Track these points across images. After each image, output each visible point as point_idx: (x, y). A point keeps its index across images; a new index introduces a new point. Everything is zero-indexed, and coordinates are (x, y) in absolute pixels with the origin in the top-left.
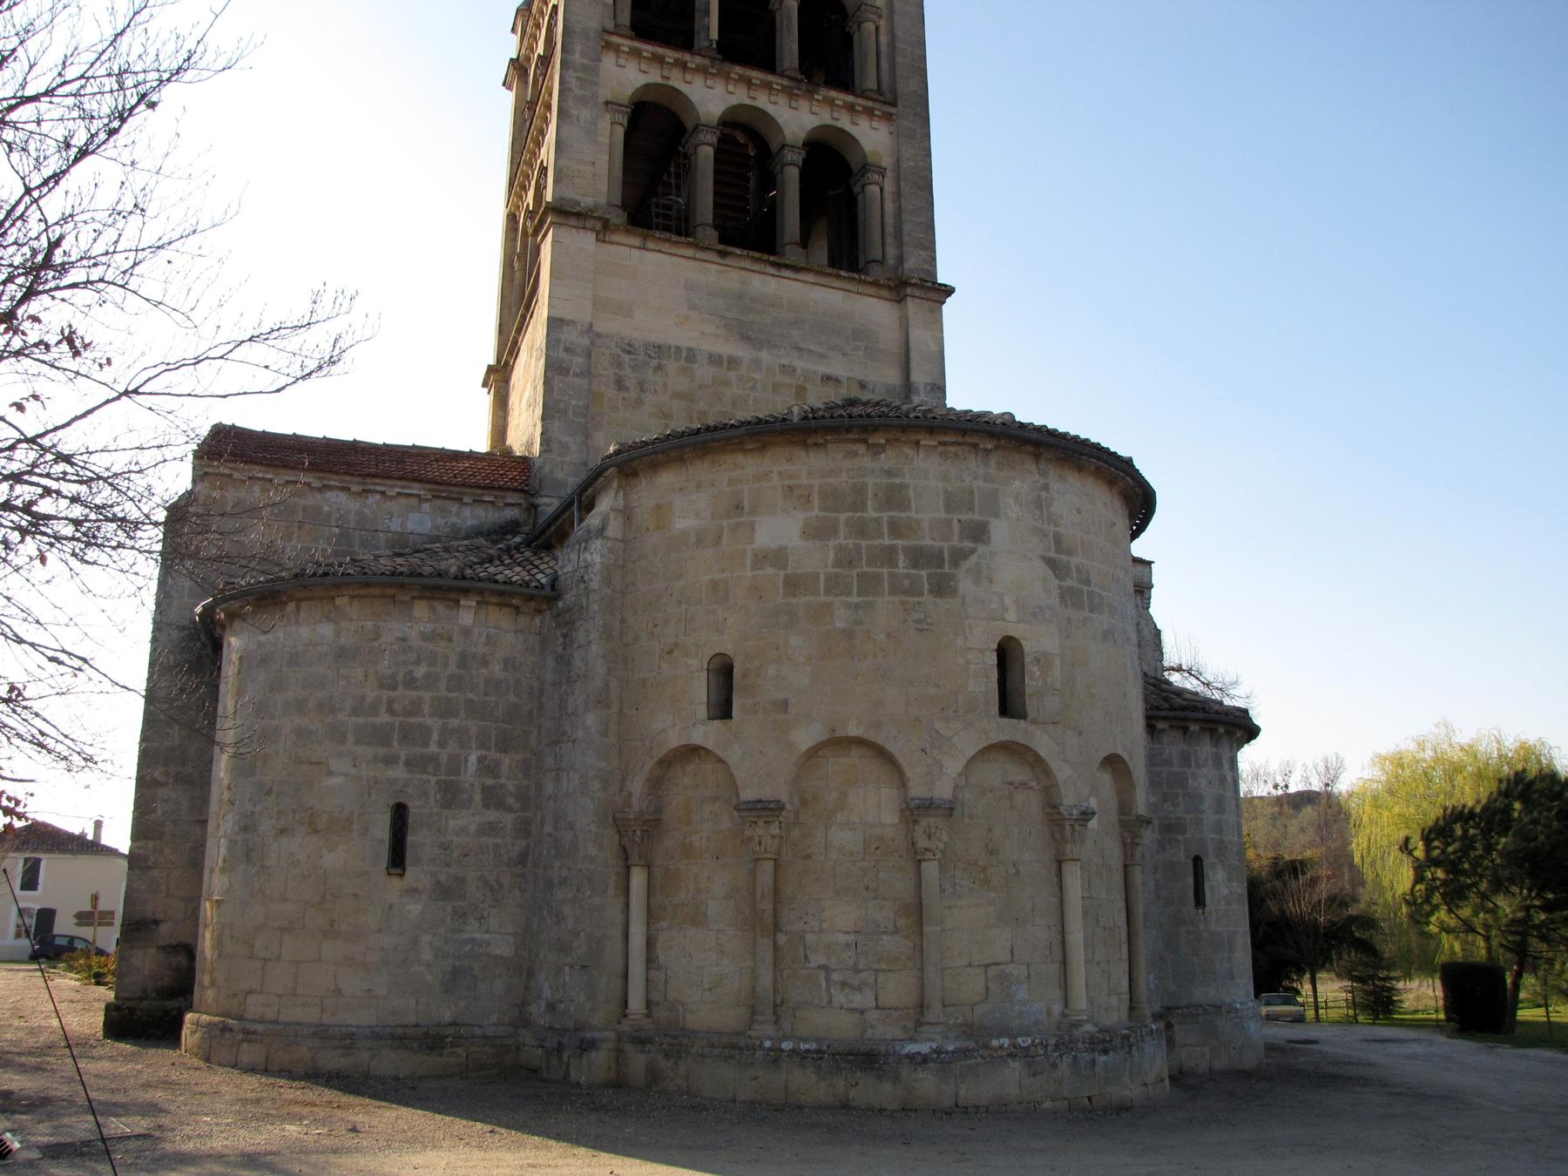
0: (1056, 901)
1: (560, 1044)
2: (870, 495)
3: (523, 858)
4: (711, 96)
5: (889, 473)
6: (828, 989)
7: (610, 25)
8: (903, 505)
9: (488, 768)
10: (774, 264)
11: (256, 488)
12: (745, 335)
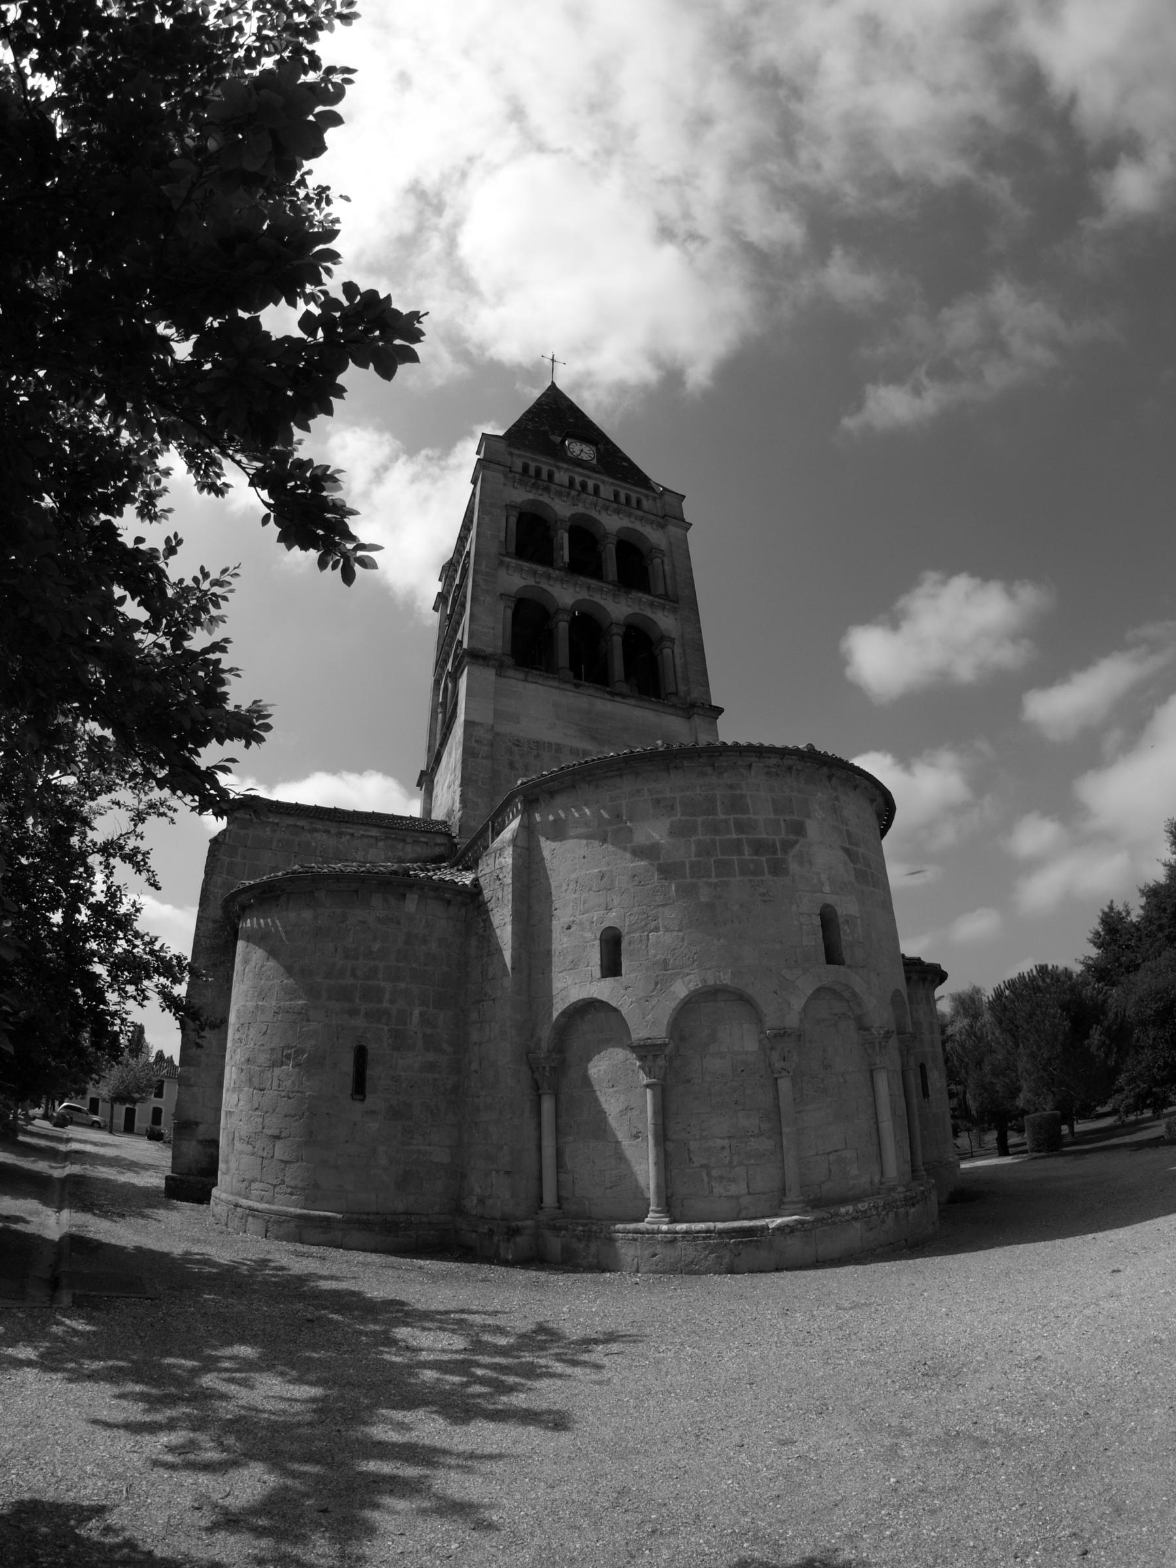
0: (870, 1099)
1: (490, 1230)
2: (718, 804)
4: (566, 594)
5: (731, 787)
6: (709, 1182)
10: (609, 693)
11: (268, 829)
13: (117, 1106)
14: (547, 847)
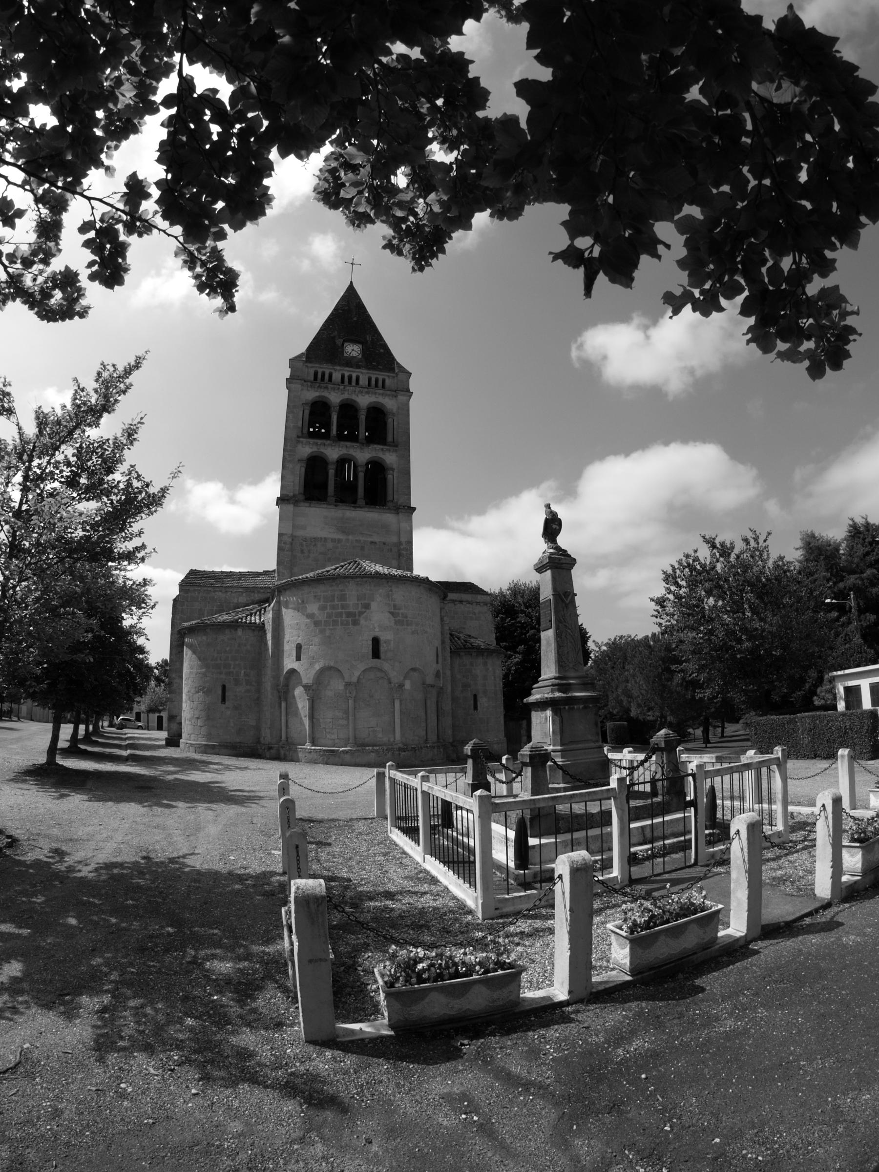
3: (258, 699)
5: (341, 591)
7: (300, 434)
8: (345, 600)
9: (246, 674)
12: (344, 531)
13: (151, 715)
14: (284, 610)
